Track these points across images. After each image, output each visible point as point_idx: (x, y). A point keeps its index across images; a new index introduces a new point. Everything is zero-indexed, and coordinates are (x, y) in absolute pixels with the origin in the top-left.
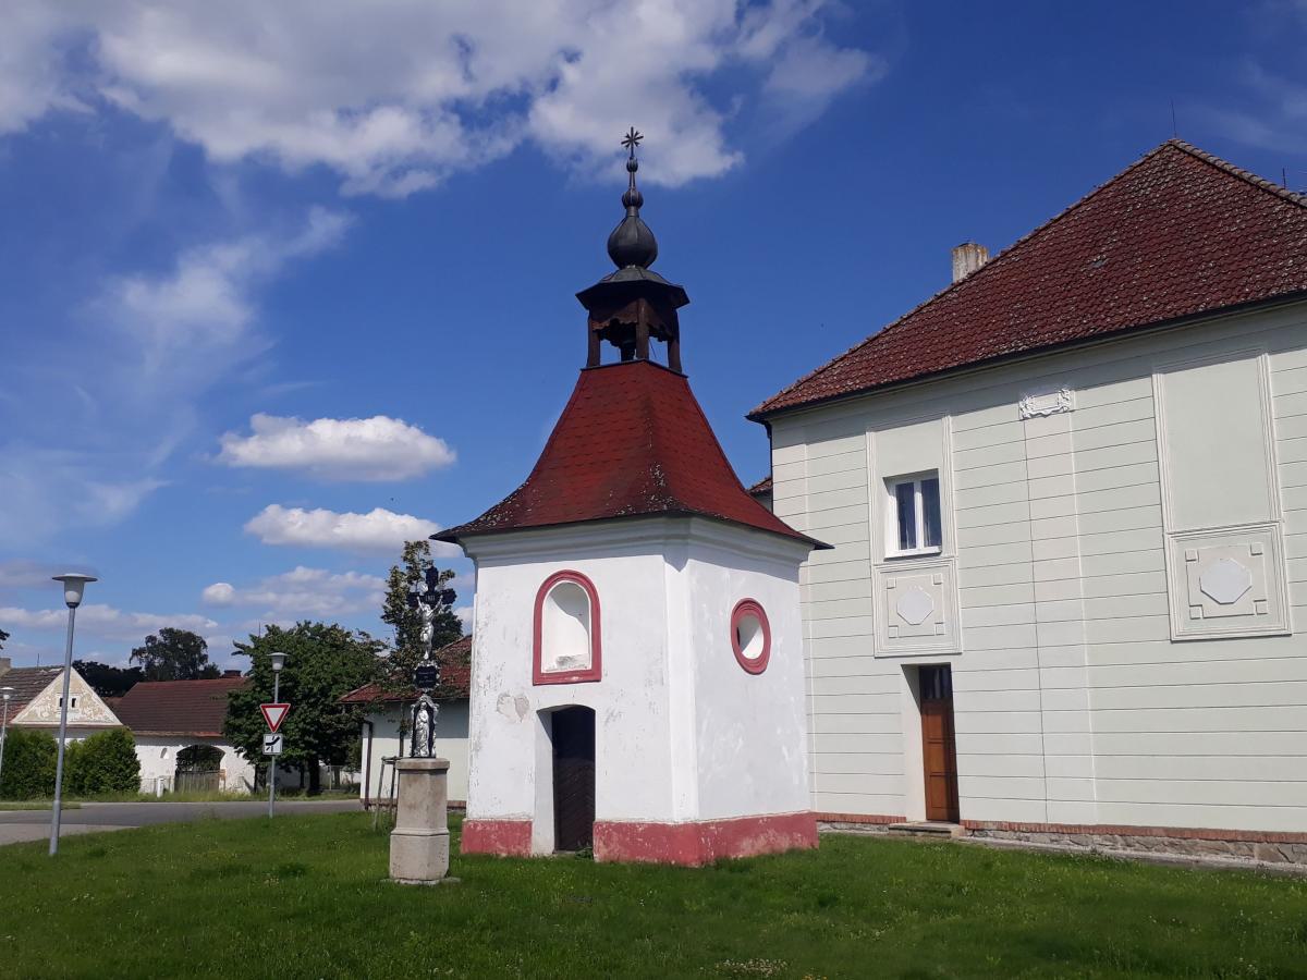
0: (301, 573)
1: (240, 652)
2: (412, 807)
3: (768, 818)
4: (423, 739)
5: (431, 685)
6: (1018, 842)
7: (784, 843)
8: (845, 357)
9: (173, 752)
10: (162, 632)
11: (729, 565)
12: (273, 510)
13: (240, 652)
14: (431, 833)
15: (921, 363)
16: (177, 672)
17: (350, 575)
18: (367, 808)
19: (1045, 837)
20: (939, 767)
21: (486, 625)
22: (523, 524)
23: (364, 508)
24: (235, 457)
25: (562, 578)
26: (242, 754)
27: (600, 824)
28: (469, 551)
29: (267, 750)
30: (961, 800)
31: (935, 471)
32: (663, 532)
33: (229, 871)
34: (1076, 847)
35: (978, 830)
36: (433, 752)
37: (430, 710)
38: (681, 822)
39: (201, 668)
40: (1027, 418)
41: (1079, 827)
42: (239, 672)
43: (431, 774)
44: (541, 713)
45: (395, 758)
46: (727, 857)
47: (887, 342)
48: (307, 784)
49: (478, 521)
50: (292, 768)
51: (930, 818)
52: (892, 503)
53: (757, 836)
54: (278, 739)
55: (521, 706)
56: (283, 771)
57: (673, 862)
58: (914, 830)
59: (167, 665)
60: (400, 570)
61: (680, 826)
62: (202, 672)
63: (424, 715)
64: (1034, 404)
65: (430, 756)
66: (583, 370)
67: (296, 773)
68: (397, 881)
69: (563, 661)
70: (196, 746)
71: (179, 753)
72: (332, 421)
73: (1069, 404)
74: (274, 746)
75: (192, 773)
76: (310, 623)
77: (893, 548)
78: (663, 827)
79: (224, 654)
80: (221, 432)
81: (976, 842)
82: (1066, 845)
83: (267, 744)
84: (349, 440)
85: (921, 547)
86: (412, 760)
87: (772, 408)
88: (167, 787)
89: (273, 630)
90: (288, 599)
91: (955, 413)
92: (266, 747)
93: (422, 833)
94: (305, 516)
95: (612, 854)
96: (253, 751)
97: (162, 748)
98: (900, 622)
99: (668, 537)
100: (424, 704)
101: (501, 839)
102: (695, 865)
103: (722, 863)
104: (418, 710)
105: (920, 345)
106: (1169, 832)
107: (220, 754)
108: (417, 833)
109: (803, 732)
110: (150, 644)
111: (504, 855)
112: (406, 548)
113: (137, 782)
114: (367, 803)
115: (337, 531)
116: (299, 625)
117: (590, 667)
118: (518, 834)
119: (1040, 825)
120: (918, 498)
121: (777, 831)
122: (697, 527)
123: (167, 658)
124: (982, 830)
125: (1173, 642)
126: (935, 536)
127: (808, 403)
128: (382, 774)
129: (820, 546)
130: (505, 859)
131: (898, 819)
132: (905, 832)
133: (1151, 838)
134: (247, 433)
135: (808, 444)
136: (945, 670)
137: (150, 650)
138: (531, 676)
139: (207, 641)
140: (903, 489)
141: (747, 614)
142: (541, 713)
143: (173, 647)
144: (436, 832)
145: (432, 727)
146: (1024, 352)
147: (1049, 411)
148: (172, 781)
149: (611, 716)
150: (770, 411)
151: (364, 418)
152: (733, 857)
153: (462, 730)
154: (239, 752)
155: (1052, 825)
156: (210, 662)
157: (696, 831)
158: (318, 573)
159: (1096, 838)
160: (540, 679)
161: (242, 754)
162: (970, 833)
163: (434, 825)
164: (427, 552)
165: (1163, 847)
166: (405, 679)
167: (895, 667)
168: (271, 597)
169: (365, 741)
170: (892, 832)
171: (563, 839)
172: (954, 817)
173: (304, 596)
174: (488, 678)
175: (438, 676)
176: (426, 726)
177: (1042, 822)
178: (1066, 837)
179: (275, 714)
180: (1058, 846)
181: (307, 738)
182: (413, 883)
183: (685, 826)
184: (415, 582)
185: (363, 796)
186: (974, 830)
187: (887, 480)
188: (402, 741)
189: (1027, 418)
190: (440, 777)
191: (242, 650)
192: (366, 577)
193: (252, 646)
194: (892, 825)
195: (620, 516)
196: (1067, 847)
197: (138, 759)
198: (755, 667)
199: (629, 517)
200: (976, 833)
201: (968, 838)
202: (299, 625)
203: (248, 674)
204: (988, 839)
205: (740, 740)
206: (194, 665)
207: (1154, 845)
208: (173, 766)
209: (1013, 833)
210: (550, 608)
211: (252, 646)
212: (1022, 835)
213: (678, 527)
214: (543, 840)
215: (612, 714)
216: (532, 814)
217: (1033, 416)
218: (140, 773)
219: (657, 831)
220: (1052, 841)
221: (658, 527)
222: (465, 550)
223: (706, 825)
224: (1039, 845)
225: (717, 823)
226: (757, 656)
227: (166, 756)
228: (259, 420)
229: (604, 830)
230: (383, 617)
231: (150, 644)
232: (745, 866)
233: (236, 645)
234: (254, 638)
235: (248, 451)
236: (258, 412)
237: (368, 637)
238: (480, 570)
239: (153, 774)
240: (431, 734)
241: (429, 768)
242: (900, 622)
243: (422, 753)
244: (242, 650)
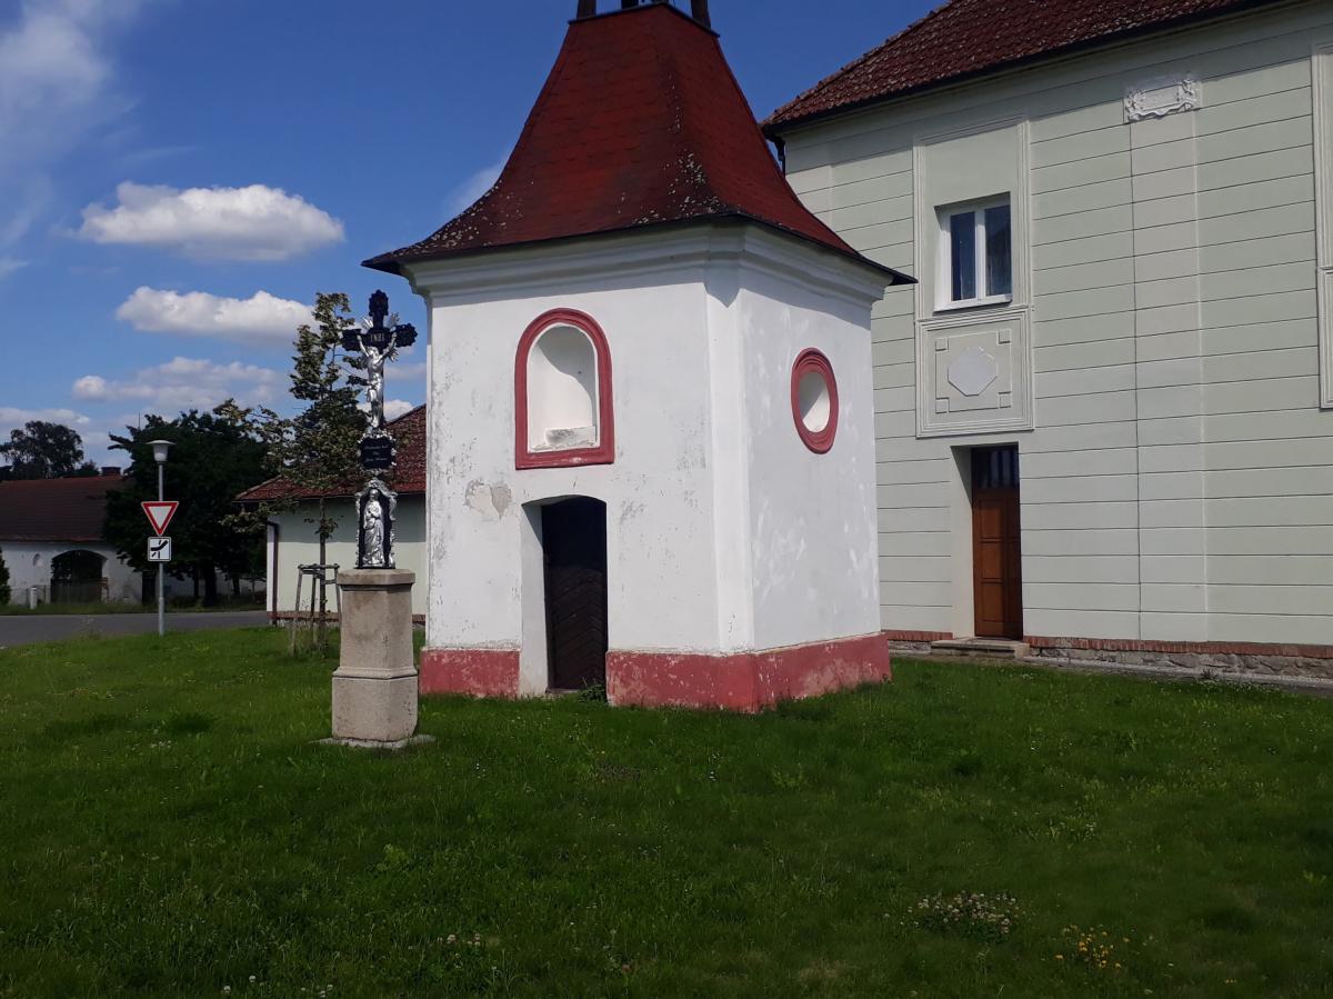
0: (181, 364)
1: (117, 446)
2: (361, 639)
3: (835, 644)
4: (375, 542)
5: (385, 465)
6: (1099, 663)
7: (853, 677)
8: (881, 50)
9: (47, 557)
10: (28, 426)
11: (789, 302)
12: (143, 293)
13: (117, 446)
14: (392, 674)
15: (989, 52)
16: (50, 469)
17: (235, 366)
18: (275, 623)
19: (1138, 657)
20: (993, 571)
21: (447, 387)
22: (498, 242)
23: (245, 294)
24: (100, 232)
25: (555, 320)
26: (126, 560)
27: (616, 655)
28: (419, 283)
29: (153, 557)
30: (1025, 613)
31: (1007, 195)
32: (703, 248)
33: (100, 725)
34: (1179, 670)
35: (1046, 648)
36: (391, 560)
37: (383, 501)
38: (731, 653)
39: (77, 466)
40: (1135, 121)
41: (1184, 644)
42: (119, 469)
43: (389, 592)
44: (529, 507)
45: (314, 567)
46: (790, 699)
47: (936, 30)
48: (202, 592)
49: (429, 241)
50: (185, 575)
51: (979, 633)
52: (945, 239)
53: (822, 670)
54: (166, 542)
55: (500, 498)
56: (174, 579)
57: (721, 707)
58: (963, 649)
59: (38, 462)
60: (311, 330)
61: (729, 659)
62: (79, 471)
63: (375, 507)
64: (1143, 101)
65: (387, 566)
66: (571, 23)
67: (189, 581)
68: (343, 742)
69: (557, 436)
70: (74, 552)
71: (56, 561)
72: (205, 191)
73: (1193, 101)
74: (160, 551)
75: (70, 582)
76: (196, 412)
77: (944, 300)
78: (707, 659)
79: (101, 451)
80: (84, 206)
81: (1047, 664)
82: (1164, 666)
83: (153, 549)
84: (225, 214)
85: (982, 296)
86: (361, 572)
87: (787, 117)
88: (42, 598)
89: (154, 421)
90: (167, 393)
91: (1035, 117)
92: (152, 553)
93: (379, 675)
94: (181, 300)
95: (633, 695)
96: (138, 557)
97: (33, 554)
98: (952, 393)
99: (710, 256)
100: (374, 492)
101: (481, 677)
102: (751, 710)
103: (786, 708)
104: (366, 500)
105: (985, 30)
106: (1305, 650)
107: (99, 561)
108: (371, 674)
109: (873, 529)
110: (16, 439)
111: (481, 696)
112: (319, 302)
113: (6, 592)
114: (276, 616)
115: (218, 318)
116: (184, 415)
117: (597, 444)
118: (501, 668)
119: (1129, 642)
120: (981, 233)
121: (846, 661)
122: (754, 241)
123: (36, 454)
124: (1054, 648)
125: (1322, 410)
126: (1001, 276)
127: (836, 110)
128: (299, 586)
129: (899, 279)
130: (483, 701)
131: (941, 636)
132: (953, 651)
133: (1279, 657)
134: (112, 205)
135: (833, 165)
136: (1006, 455)
137: (17, 446)
138: (513, 457)
139: (82, 438)
140: (959, 220)
141: (813, 371)
142: (529, 507)
143: (42, 442)
144: (397, 674)
145: (388, 525)
146: (1135, 32)
147: (1164, 111)
148: (48, 592)
149: (629, 510)
150: (785, 121)
151: (237, 187)
152: (797, 698)
153: (417, 532)
154: (123, 558)
155: (1147, 643)
156: (86, 460)
157: (751, 664)
158: (199, 364)
159: (1205, 658)
160: (525, 461)
161: (126, 560)
162: (1035, 653)
163: (395, 664)
164: (345, 308)
165: (1296, 669)
166: (325, 469)
167: (944, 449)
168: (146, 391)
169: (270, 546)
170: (936, 651)
171: (557, 677)
172: (1013, 629)
173: (185, 390)
174: (452, 460)
175: (394, 451)
176: (379, 523)
177: (1134, 638)
178: (1166, 657)
179: (160, 514)
180: (1155, 668)
181: (200, 543)
182: (368, 745)
183: (737, 658)
184: (332, 346)
185: (269, 608)
186: (1041, 649)
187: (939, 210)
188: (323, 545)
189: (1135, 121)
190: (400, 595)
191: (122, 443)
192: (251, 369)
193: (131, 439)
194: (935, 643)
195: (640, 226)
196: (1167, 670)
197: (6, 566)
198: (819, 443)
199: (654, 227)
200: (1044, 651)
201: (1036, 659)
202: (184, 415)
203: (127, 471)
204: (1062, 660)
205: (802, 541)
206: (67, 461)
207: (1282, 667)
208: (49, 575)
209: (1093, 652)
210: (537, 362)
211: (131, 439)
212: (1105, 654)
213: (727, 242)
214: (534, 677)
215: (630, 508)
216: (519, 641)
217: (1142, 118)
218: (10, 582)
219: (697, 666)
220: (1146, 662)
221: (696, 241)
222: (412, 282)
223: (764, 657)
224: (1130, 666)
225: (777, 653)
226: (822, 428)
227: (40, 563)
228: (126, 190)
229: (621, 663)
230: (292, 390)
231: (16, 439)
232: (818, 711)
233: (113, 438)
234: (133, 430)
235: (117, 226)
236: (123, 179)
237: (274, 416)
238: (434, 310)
239: (26, 583)
240: (387, 535)
241: (387, 582)
242: (952, 393)
243: (375, 562)
244: (122, 443)
